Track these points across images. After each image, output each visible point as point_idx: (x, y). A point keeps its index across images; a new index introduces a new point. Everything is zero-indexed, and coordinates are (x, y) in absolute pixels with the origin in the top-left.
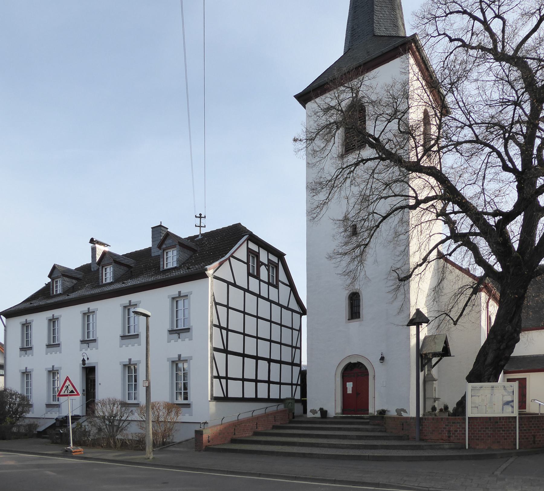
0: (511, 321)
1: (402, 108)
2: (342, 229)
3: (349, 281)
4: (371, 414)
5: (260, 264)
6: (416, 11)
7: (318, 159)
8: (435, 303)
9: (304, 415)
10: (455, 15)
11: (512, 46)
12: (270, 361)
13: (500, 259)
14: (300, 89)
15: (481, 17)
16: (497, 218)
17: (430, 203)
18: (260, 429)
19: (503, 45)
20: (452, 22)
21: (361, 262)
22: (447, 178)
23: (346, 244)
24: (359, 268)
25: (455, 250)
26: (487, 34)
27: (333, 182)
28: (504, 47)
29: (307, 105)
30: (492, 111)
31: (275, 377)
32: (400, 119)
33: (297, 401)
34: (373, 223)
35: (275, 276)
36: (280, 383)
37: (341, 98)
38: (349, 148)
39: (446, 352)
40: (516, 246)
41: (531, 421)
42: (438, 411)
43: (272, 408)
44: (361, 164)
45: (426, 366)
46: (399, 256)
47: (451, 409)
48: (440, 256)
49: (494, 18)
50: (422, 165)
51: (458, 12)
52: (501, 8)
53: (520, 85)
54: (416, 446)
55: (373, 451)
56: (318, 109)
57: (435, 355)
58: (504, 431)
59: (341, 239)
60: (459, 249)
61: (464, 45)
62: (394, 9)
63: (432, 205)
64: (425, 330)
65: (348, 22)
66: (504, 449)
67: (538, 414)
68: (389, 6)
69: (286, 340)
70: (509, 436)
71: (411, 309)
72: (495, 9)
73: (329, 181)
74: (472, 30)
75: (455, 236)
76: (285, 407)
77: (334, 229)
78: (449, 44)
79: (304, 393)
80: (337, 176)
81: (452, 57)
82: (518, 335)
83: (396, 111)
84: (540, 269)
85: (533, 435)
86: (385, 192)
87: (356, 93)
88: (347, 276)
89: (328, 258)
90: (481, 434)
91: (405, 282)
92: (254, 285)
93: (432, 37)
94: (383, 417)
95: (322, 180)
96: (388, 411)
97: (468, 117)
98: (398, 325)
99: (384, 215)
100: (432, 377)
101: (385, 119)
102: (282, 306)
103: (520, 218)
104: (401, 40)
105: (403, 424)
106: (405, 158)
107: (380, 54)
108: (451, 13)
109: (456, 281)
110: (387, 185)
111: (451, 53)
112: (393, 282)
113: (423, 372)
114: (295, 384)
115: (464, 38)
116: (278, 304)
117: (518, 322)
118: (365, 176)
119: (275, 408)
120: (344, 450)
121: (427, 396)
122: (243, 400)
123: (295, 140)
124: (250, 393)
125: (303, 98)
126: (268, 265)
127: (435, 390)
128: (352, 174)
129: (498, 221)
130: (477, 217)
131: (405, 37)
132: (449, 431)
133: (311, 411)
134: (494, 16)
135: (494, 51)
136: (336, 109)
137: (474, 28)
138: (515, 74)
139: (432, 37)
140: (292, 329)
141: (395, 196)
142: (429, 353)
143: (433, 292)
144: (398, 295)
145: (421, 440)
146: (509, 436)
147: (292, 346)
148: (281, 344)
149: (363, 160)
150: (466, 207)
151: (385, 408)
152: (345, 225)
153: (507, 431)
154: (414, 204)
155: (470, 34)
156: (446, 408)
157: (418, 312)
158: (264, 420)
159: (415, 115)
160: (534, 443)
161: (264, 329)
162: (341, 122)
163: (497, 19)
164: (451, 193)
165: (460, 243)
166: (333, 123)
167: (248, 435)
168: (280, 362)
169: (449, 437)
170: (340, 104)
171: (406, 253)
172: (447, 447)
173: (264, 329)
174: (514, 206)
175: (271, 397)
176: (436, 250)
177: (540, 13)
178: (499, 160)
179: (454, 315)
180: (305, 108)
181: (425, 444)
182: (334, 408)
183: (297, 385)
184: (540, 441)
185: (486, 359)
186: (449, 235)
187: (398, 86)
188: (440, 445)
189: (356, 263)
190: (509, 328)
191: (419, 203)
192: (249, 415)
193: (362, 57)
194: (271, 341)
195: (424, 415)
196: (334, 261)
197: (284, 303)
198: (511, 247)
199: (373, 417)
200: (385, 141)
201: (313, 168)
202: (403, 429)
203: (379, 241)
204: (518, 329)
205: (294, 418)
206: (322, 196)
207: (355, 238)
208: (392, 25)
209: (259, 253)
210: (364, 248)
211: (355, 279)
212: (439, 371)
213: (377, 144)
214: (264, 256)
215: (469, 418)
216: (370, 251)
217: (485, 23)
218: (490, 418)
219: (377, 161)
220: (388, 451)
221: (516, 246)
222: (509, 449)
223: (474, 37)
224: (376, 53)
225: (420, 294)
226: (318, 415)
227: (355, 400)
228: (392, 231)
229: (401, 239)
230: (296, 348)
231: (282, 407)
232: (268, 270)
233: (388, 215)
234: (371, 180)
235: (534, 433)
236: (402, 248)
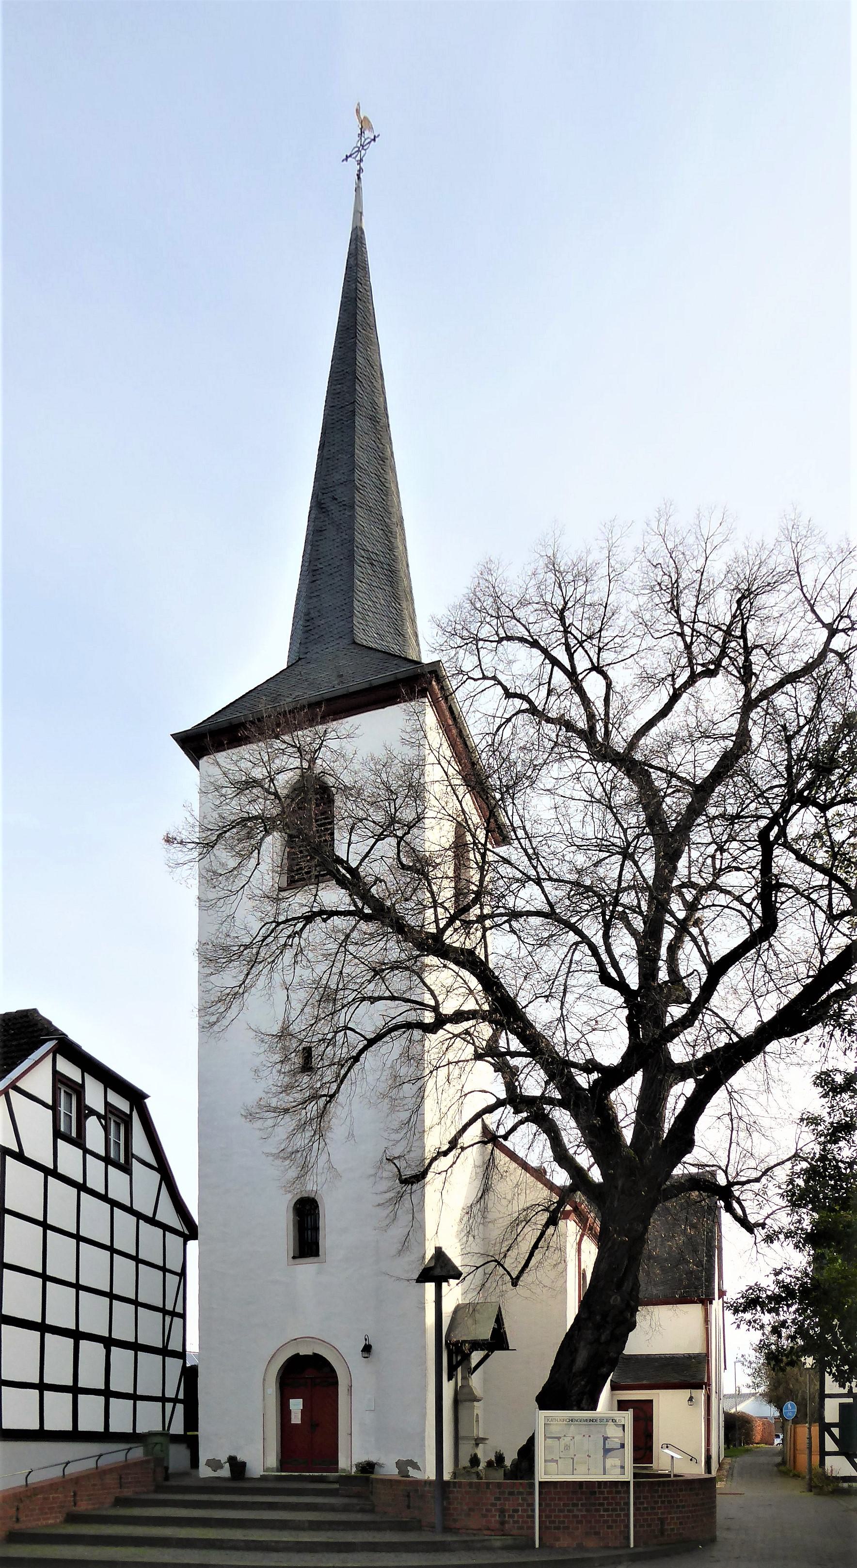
0: (619, 1286)
1: (408, 815)
2: (277, 1057)
3: (293, 1173)
4: (344, 1470)
5: (84, 1112)
6: (439, 617)
7: (222, 894)
8: (471, 1238)
9: (193, 1471)
10: (517, 645)
11: (624, 734)
12: (109, 1342)
13: (600, 1159)
14: (189, 721)
15: (564, 660)
16: (595, 1076)
17: (466, 1025)
18: (84, 1506)
19: (606, 727)
20: (511, 658)
21: (320, 1133)
22: (497, 977)
23: (287, 1089)
24: (316, 1145)
25: (514, 1129)
26: (577, 699)
27: (254, 951)
28: (607, 733)
29: (202, 762)
30: (581, 860)
31: (121, 1382)
32: (400, 839)
33: (176, 1439)
34: (345, 1050)
35: (122, 1142)
36: (134, 1397)
37: (274, 767)
38: (295, 877)
39: (498, 1341)
40: (628, 1135)
41: (657, 1491)
42: (483, 1465)
43: (114, 1455)
44: (318, 920)
45: (459, 1369)
46: (397, 1131)
47: (508, 1463)
48: (490, 1138)
49: (591, 670)
50: (448, 942)
51: (522, 640)
52: (603, 655)
53: (634, 818)
54: (434, 1543)
55: (343, 1556)
56: (223, 781)
57: (476, 1345)
58: (606, 1510)
59: (273, 1078)
60: (523, 1127)
61: (533, 710)
62: (396, 598)
63: (467, 1032)
64: (454, 1294)
65: (298, 599)
66: (607, 1547)
67: (668, 1476)
68: (386, 588)
69: (150, 1293)
70: (615, 1521)
71: (427, 1243)
72: (591, 655)
73: (246, 947)
74: (549, 683)
75: (515, 1099)
76: (146, 1453)
77: (259, 1054)
78: (504, 702)
79: (191, 1420)
80: (265, 938)
81: (507, 732)
82: (633, 1315)
83: (393, 820)
84: (672, 1186)
85: (659, 1519)
86: (371, 986)
87: (309, 762)
88: (287, 1162)
89: (246, 1117)
90: (565, 1516)
91: (415, 1187)
92: (70, 1160)
93: (469, 678)
94: (367, 1479)
95: (229, 941)
96: (381, 1466)
97: (534, 862)
98: (399, 1279)
99: (371, 1036)
100: (471, 1392)
101: (370, 834)
102: (139, 1216)
103: (636, 1081)
104: (405, 668)
105: (408, 1496)
106: (411, 921)
107: (366, 686)
108: (509, 638)
109: (520, 1194)
110: (377, 972)
111: (509, 720)
112: (388, 1183)
113: (452, 1382)
114: (170, 1400)
115: (532, 696)
116: (130, 1210)
117: (632, 1289)
118: (330, 946)
119: (120, 1457)
120: (281, 1555)
121: (462, 1433)
122: (41, 1435)
123: (169, 840)
124: (58, 1417)
125: (197, 743)
126: (105, 1117)
127: (477, 1421)
128: (296, 940)
129: (595, 1081)
130: (558, 1068)
131: (420, 663)
132: (502, 1511)
133: (209, 1463)
134: (590, 666)
135: (588, 736)
136: (262, 787)
137: (553, 681)
138: (626, 791)
139: (469, 678)
140: (164, 1269)
141: (393, 998)
142: (464, 1342)
143: (467, 1217)
144: (399, 1212)
145: (446, 1530)
146: (615, 1521)
147: (163, 1311)
148: (136, 1303)
149: (321, 913)
150: (536, 1045)
151: (373, 1459)
152: (284, 1048)
153: (613, 1510)
154: (432, 1021)
155: (544, 690)
156: (500, 1458)
157: (439, 1253)
158: (94, 1485)
159: (436, 836)
160: (662, 1532)
161: (95, 1267)
162: (273, 819)
163: (594, 673)
164: (505, 1011)
165: (525, 1115)
166: (256, 818)
167: (52, 1522)
168: (135, 1347)
169: (503, 1523)
170: (272, 780)
171: (413, 1125)
172: (498, 1544)
173: (95, 1267)
174: (623, 1058)
175: (111, 1430)
176: (478, 1124)
177: (673, 680)
178: (593, 961)
179: (513, 1264)
180: (198, 767)
181: (455, 1538)
182: (261, 1456)
183: (175, 1401)
184: (672, 1530)
185: (573, 1361)
186: (503, 1095)
187: (397, 768)
188: (484, 1540)
189: (308, 1134)
190: (616, 1300)
191: (441, 1021)
192: (56, 1473)
193: (326, 682)
194: (111, 1296)
195: (455, 1475)
196: (259, 1124)
197: (145, 1206)
198: (619, 1136)
199: (347, 1479)
200: (370, 879)
201: (210, 912)
202: (409, 1507)
203: (358, 1090)
204: (632, 1303)
205: (167, 1478)
206: (230, 978)
207: (306, 1079)
208: (392, 631)
209: (83, 1086)
210: (328, 1102)
211: (305, 1169)
212: (485, 1380)
213: (353, 881)
214: (95, 1095)
215: (540, 1483)
216: (337, 1110)
217: (572, 675)
218: (581, 1484)
219: (352, 920)
220: (377, 1555)
221: (628, 1135)
222: (616, 1548)
223: (552, 699)
224: (357, 682)
225: (445, 1217)
226: (225, 1472)
227: (309, 1440)
228: (387, 1073)
229: (407, 1093)
230: (173, 1314)
231: (138, 1453)
232: (106, 1129)
233: (379, 1037)
234: (340, 956)
235: (663, 1513)
236: (405, 1116)
